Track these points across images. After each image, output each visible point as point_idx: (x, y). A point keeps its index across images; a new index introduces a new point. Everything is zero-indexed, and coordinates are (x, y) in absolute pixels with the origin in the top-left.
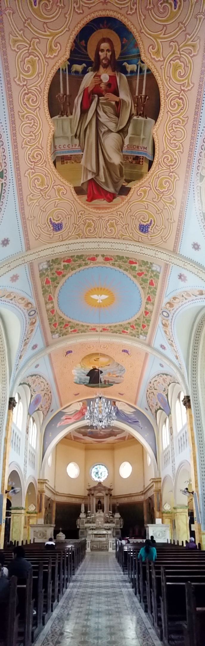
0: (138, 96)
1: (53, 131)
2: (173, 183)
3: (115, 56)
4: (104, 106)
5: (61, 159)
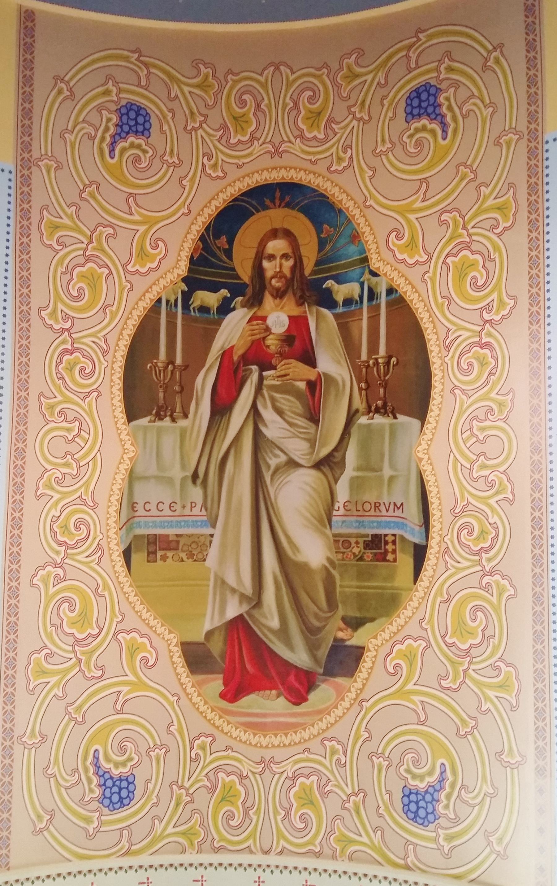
0: (368, 362)
1: (131, 459)
2: (497, 610)
3: (302, 269)
4: (277, 395)
5: (149, 543)
